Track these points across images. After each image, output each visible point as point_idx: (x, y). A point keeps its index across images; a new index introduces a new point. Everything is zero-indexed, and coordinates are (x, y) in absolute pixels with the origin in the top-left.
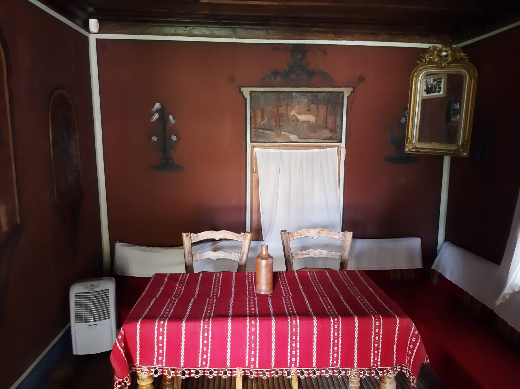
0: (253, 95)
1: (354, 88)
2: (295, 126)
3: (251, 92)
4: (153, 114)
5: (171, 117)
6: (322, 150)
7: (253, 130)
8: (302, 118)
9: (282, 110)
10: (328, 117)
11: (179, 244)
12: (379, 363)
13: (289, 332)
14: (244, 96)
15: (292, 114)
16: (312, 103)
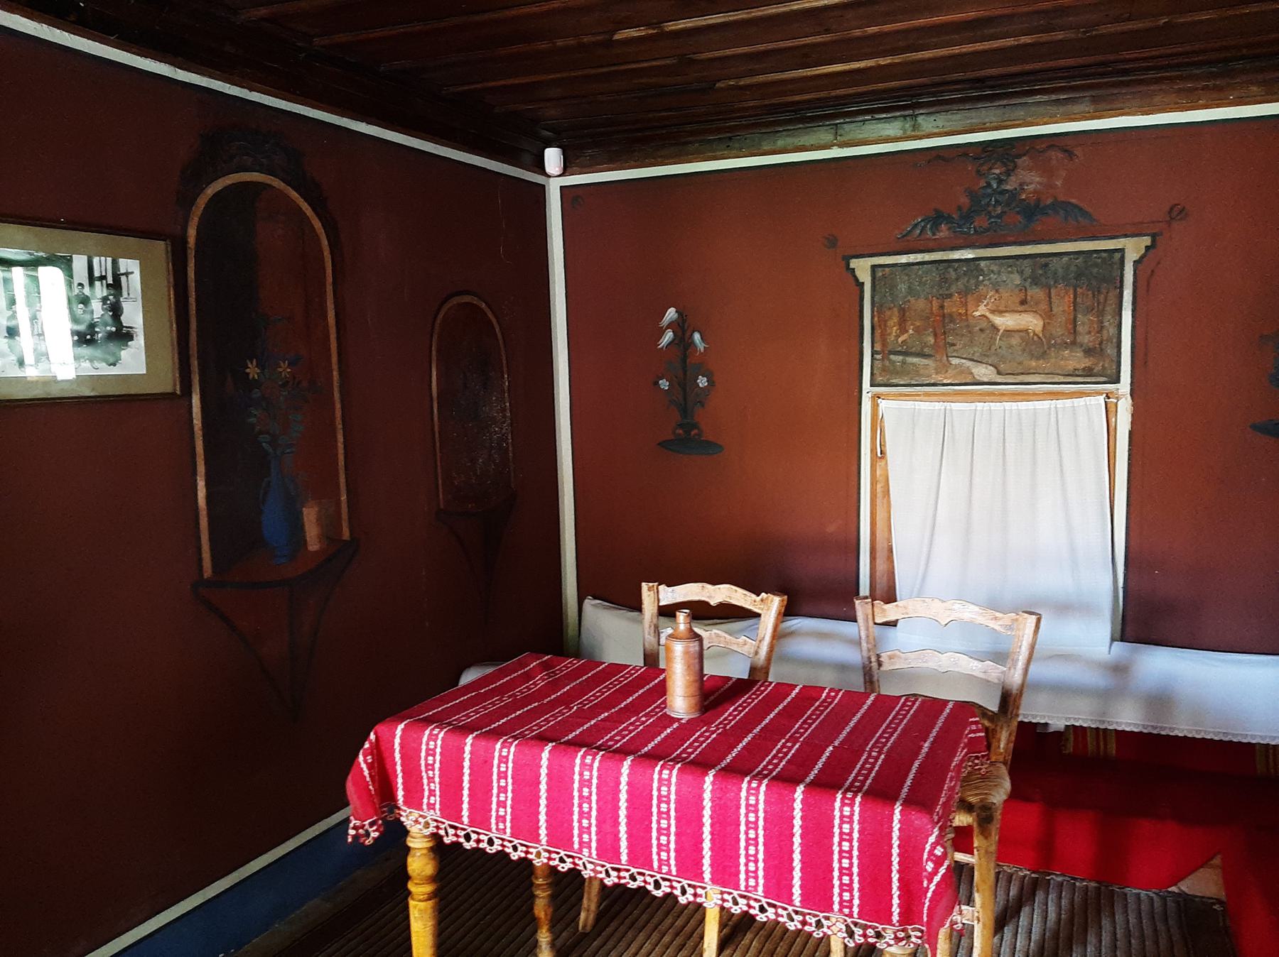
1: (1154, 236)
2: (988, 344)
3: (874, 267)
4: (661, 332)
5: (697, 336)
6: (1060, 403)
7: (878, 357)
8: (1005, 322)
9: (951, 307)
12: (856, 910)
14: (856, 279)
15: (977, 314)
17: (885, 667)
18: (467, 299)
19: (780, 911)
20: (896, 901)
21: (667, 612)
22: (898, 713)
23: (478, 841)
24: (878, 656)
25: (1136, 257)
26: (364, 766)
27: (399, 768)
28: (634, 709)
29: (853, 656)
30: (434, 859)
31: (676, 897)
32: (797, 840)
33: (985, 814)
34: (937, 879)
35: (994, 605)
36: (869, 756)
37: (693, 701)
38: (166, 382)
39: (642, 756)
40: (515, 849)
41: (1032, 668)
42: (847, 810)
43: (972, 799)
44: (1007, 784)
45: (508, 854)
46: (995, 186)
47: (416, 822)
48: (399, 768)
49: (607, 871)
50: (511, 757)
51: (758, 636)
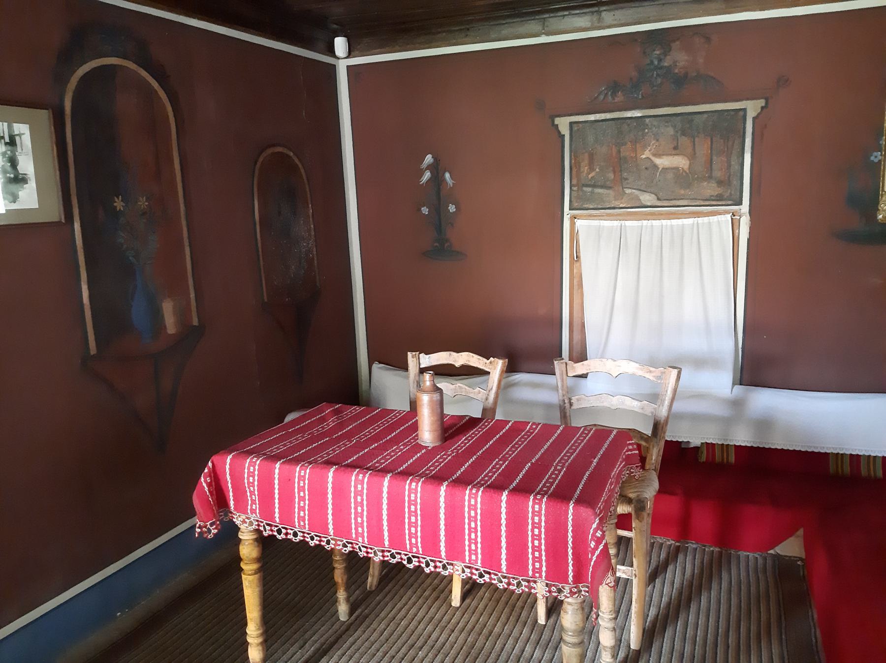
0: (575, 128)
2: (651, 180)
3: (571, 124)
4: (422, 174)
5: (447, 175)
6: (700, 220)
7: (575, 188)
8: (663, 162)
9: (626, 151)
10: (715, 158)
11: (403, 366)
12: (544, 574)
13: (407, 499)
14: (559, 132)
15: (644, 156)
17: (575, 407)
18: (279, 149)
20: (571, 568)
21: (422, 371)
22: (578, 439)
23: (287, 534)
24: (570, 399)
25: (754, 114)
26: (204, 485)
27: (230, 485)
28: (395, 441)
29: (553, 398)
31: (423, 568)
32: (503, 528)
33: (640, 506)
34: (597, 552)
35: (652, 362)
36: (555, 469)
37: (436, 434)
38: (55, 213)
39: (399, 473)
40: (312, 538)
41: (675, 405)
42: (537, 507)
43: (632, 496)
44: (656, 485)
45: (308, 542)
46: (656, 63)
47: (244, 522)
48: (230, 485)
49: (375, 552)
51: (484, 388)
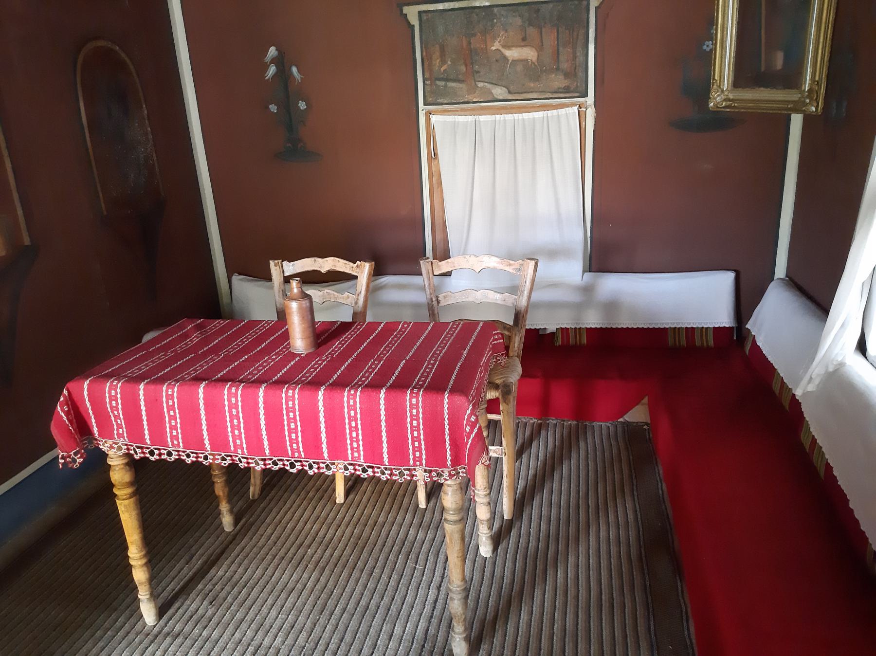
0: (424, 17)
2: (503, 74)
3: (420, 13)
4: (266, 67)
5: (294, 70)
6: (549, 113)
7: (428, 82)
8: (512, 54)
9: (476, 43)
10: (561, 49)
11: (267, 277)
12: (424, 462)
13: (284, 406)
14: (409, 23)
15: (493, 48)
16: (530, 24)
17: (442, 304)
19: (376, 470)
21: (287, 280)
22: (448, 333)
24: (437, 297)
25: (596, 4)
29: (421, 298)
30: (130, 470)
33: (506, 390)
35: (510, 256)
39: (274, 382)
40: (188, 456)
41: (533, 294)
43: (498, 382)
44: (519, 370)
47: (111, 447)
50: (175, 395)
51: (354, 293)
